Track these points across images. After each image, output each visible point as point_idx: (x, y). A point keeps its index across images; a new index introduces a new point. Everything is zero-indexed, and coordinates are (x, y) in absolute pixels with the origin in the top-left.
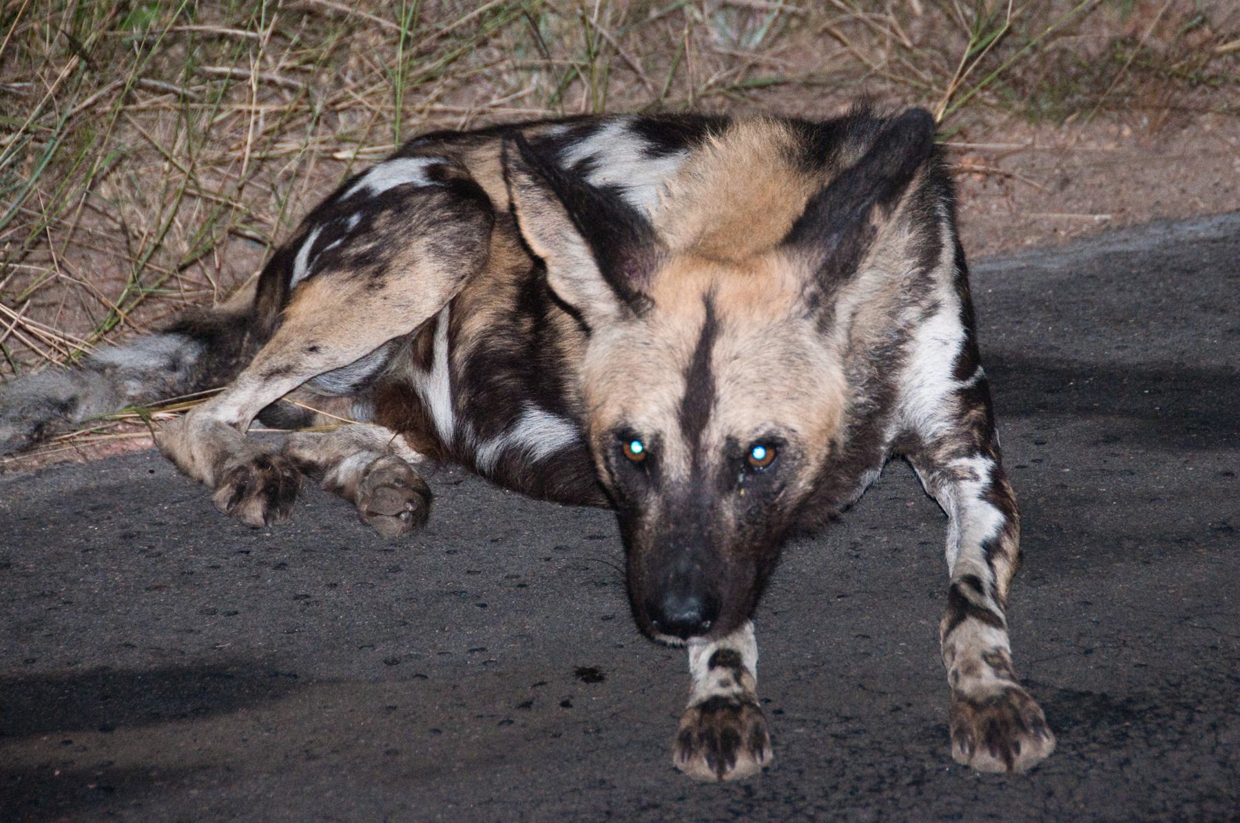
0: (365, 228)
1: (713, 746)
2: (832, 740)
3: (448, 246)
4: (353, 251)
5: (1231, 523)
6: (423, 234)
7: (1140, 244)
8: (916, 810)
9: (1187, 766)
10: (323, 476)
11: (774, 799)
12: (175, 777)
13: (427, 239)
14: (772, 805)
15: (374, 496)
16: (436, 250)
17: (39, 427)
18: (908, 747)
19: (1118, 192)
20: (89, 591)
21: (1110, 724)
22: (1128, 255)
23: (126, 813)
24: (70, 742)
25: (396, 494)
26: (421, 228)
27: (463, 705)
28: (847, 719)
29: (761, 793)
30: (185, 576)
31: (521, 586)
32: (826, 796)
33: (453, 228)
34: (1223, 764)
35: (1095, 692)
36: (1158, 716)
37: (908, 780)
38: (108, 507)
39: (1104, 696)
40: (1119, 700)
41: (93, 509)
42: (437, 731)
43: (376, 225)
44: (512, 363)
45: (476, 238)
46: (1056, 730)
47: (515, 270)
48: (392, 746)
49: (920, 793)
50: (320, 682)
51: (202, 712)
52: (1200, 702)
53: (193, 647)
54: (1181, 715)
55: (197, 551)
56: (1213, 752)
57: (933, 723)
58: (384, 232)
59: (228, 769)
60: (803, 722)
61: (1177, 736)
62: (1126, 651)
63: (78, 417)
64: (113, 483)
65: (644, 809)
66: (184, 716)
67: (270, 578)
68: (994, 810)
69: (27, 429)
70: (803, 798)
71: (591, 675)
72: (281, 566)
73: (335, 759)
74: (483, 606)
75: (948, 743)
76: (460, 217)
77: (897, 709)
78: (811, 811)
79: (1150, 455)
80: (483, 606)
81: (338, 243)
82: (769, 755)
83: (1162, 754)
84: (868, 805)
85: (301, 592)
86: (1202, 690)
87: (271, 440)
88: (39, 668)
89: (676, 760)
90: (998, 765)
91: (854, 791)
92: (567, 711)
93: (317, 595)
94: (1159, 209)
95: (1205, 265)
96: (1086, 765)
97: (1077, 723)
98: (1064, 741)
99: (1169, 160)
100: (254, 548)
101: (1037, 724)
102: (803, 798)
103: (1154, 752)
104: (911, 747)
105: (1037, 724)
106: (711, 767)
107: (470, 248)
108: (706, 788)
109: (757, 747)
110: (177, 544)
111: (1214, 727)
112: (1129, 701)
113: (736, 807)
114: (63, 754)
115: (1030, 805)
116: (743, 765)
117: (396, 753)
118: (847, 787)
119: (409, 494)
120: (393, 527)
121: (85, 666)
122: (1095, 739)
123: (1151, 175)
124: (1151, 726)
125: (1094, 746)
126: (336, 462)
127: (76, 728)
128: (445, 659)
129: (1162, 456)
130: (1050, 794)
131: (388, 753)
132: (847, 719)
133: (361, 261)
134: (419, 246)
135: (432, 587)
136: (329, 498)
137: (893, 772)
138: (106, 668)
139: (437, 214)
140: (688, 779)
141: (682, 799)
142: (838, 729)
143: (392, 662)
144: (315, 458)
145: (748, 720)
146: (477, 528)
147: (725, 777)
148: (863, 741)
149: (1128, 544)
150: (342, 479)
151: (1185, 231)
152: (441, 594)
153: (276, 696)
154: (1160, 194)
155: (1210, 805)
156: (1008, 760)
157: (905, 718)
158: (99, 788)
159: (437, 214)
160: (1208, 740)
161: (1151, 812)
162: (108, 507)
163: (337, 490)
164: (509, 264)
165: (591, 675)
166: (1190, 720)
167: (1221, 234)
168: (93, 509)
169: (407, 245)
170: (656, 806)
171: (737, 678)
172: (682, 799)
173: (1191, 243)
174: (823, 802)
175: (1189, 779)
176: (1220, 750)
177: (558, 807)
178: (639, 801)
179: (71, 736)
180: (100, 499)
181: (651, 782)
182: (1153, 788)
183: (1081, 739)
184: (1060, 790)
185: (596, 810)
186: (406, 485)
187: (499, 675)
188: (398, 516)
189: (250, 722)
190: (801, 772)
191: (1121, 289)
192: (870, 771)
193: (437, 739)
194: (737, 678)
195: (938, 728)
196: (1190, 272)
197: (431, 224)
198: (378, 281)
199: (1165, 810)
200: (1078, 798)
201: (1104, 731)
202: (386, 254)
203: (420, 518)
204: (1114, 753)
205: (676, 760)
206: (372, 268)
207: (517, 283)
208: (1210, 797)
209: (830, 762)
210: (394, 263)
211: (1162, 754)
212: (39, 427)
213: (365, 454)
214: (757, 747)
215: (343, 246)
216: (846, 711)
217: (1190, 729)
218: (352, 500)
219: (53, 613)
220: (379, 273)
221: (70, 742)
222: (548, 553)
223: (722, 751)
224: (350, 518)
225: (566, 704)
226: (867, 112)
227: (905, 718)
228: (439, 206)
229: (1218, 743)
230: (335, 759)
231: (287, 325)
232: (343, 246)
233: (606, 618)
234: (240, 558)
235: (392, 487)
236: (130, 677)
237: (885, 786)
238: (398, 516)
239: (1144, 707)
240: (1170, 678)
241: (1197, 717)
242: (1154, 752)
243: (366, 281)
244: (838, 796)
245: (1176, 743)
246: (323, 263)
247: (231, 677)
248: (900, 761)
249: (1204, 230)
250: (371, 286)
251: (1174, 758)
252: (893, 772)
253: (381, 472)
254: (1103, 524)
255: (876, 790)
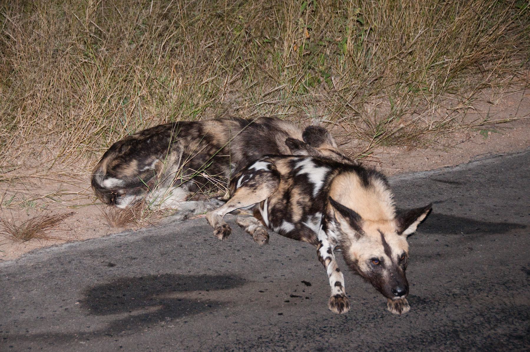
0: (253, 178)
1: (338, 306)
2: (362, 305)
3: (270, 186)
4: (250, 183)
5: (440, 253)
6: (265, 182)
7: (409, 178)
8: (383, 325)
9: (440, 317)
10: (245, 229)
11: (352, 320)
12: (224, 304)
13: (266, 184)
14: (351, 321)
15: (257, 236)
16: (268, 186)
17: (186, 216)
18: (379, 308)
19: (401, 164)
20: (199, 254)
21: (422, 304)
22: (406, 181)
23: (214, 313)
24: (200, 293)
25: (262, 236)
26: (265, 181)
27: (281, 290)
28: (365, 299)
29: (349, 318)
30: (219, 252)
31: (290, 259)
32: (363, 319)
33: (272, 182)
34: (447, 317)
35: (417, 296)
36: (431, 303)
37: (380, 316)
38: (200, 232)
39: (419, 297)
40: (422, 298)
41: (197, 232)
42: (277, 296)
43: (256, 178)
44: (281, 211)
45: (276, 185)
46: (410, 305)
47: (284, 189)
48: (268, 299)
49: (383, 320)
50: (251, 282)
51: (227, 288)
52: (440, 300)
53: (223, 270)
54: (437, 303)
55: (220, 245)
56: (445, 313)
57: (383, 302)
58: (257, 180)
59: (235, 303)
60: (355, 299)
61: (436, 309)
62: (422, 285)
63: (195, 213)
64: (200, 225)
65: (324, 320)
66: (223, 288)
67: (237, 253)
68: (400, 326)
69: (183, 216)
70: (358, 320)
71: (308, 284)
72: (238, 250)
73: (257, 302)
74: (283, 264)
75: (387, 307)
76: (273, 180)
77: (375, 297)
78: (360, 323)
79: (420, 234)
80: (283, 264)
81: (247, 180)
82: (350, 308)
83: (434, 313)
84: (372, 322)
85: (244, 258)
86: (440, 297)
87: (232, 218)
88: (192, 273)
89: (330, 308)
90: (398, 313)
91: (369, 318)
92: (304, 293)
93: (247, 259)
94: (410, 168)
95: (423, 185)
96: (418, 315)
97: (414, 304)
98: (412, 308)
99: (411, 157)
100: (232, 245)
101: (406, 304)
102: (358, 320)
103: (432, 313)
104: (379, 307)
105: (406, 304)
106: (338, 310)
107: (275, 187)
108: (337, 316)
109: (347, 306)
110: (216, 243)
111: (444, 307)
112: (425, 299)
113: (344, 321)
114: (200, 296)
115: (407, 325)
116: (345, 310)
117: (269, 301)
118: (366, 317)
119: (265, 236)
120: (261, 243)
121: (202, 273)
122: (419, 308)
123: (408, 160)
124: (431, 306)
125: (419, 310)
126: (248, 226)
127: (201, 290)
128: (276, 277)
129: (422, 235)
130: (411, 322)
131: (267, 301)
132: (365, 299)
133: (252, 186)
134: (264, 185)
135: (271, 258)
136: (246, 234)
137: (376, 314)
138: (205, 275)
139: (269, 178)
140: (333, 313)
141: (332, 318)
142: (363, 302)
143: (265, 278)
144: (243, 224)
145: (346, 300)
146: (279, 244)
147: (341, 313)
148: (369, 306)
149: (418, 257)
150: (249, 230)
151: (417, 175)
152: (273, 260)
153: (242, 285)
154: (410, 165)
155: (446, 327)
156: (400, 312)
157: (377, 300)
158: (208, 306)
159: (269, 178)
160: (443, 310)
161: (434, 328)
162: (200, 232)
163: (248, 232)
164: (282, 187)
165: (308, 284)
166: (439, 305)
167: (425, 177)
168: (197, 232)
169: (262, 184)
170: (326, 320)
171: (341, 288)
172: (332, 318)
173: (419, 178)
174: (362, 321)
175: (440, 320)
176: (446, 313)
177: (305, 318)
178: (323, 318)
179: (200, 292)
180: (198, 230)
181: (324, 313)
182: (433, 322)
183: (416, 308)
184: (413, 321)
185: (314, 320)
186: (264, 234)
187: (288, 282)
188: (262, 241)
189: (237, 291)
190: (356, 313)
191: (406, 190)
192: (371, 313)
193: (277, 298)
194: (341, 288)
195: (384, 303)
196: (420, 186)
197: (267, 180)
198: (255, 191)
199: (437, 328)
200: (417, 324)
201: (420, 306)
202: (257, 185)
203: (267, 242)
204: (423, 312)
205: (330, 308)
206: (254, 188)
207: (284, 192)
208: (446, 325)
209: (362, 310)
210: (258, 187)
211: (434, 313)
212: (186, 216)
213: (254, 225)
214: (347, 306)
215: (248, 182)
216: (364, 297)
217: (439, 307)
218: (252, 235)
219: (193, 259)
220: (255, 189)
221: (200, 293)
222: (294, 251)
223: (341, 307)
224: (251, 239)
225: (304, 291)
226: (360, 166)
227: (377, 300)
228: (269, 177)
229: (445, 311)
230: (257, 302)
231: (235, 196)
232: (248, 182)
233: (309, 269)
234: (229, 248)
235: (261, 234)
236: (210, 277)
237: (375, 318)
238: (262, 241)
239: (428, 300)
240: (433, 293)
241: (440, 304)
242: (432, 313)
243: (252, 190)
244: (365, 320)
245: (436, 310)
246: (244, 184)
247: (232, 279)
248: (377, 311)
249: (421, 175)
250: (253, 192)
251: (437, 314)
252: (376, 314)
253: (259, 231)
254: (412, 252)
255: (373, 319)
